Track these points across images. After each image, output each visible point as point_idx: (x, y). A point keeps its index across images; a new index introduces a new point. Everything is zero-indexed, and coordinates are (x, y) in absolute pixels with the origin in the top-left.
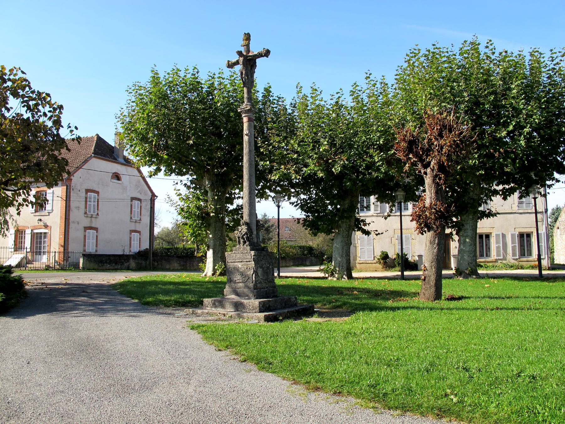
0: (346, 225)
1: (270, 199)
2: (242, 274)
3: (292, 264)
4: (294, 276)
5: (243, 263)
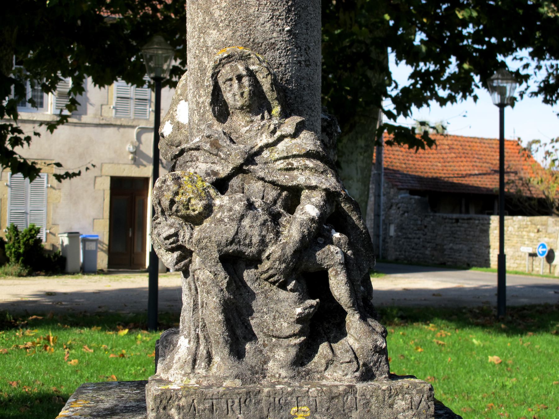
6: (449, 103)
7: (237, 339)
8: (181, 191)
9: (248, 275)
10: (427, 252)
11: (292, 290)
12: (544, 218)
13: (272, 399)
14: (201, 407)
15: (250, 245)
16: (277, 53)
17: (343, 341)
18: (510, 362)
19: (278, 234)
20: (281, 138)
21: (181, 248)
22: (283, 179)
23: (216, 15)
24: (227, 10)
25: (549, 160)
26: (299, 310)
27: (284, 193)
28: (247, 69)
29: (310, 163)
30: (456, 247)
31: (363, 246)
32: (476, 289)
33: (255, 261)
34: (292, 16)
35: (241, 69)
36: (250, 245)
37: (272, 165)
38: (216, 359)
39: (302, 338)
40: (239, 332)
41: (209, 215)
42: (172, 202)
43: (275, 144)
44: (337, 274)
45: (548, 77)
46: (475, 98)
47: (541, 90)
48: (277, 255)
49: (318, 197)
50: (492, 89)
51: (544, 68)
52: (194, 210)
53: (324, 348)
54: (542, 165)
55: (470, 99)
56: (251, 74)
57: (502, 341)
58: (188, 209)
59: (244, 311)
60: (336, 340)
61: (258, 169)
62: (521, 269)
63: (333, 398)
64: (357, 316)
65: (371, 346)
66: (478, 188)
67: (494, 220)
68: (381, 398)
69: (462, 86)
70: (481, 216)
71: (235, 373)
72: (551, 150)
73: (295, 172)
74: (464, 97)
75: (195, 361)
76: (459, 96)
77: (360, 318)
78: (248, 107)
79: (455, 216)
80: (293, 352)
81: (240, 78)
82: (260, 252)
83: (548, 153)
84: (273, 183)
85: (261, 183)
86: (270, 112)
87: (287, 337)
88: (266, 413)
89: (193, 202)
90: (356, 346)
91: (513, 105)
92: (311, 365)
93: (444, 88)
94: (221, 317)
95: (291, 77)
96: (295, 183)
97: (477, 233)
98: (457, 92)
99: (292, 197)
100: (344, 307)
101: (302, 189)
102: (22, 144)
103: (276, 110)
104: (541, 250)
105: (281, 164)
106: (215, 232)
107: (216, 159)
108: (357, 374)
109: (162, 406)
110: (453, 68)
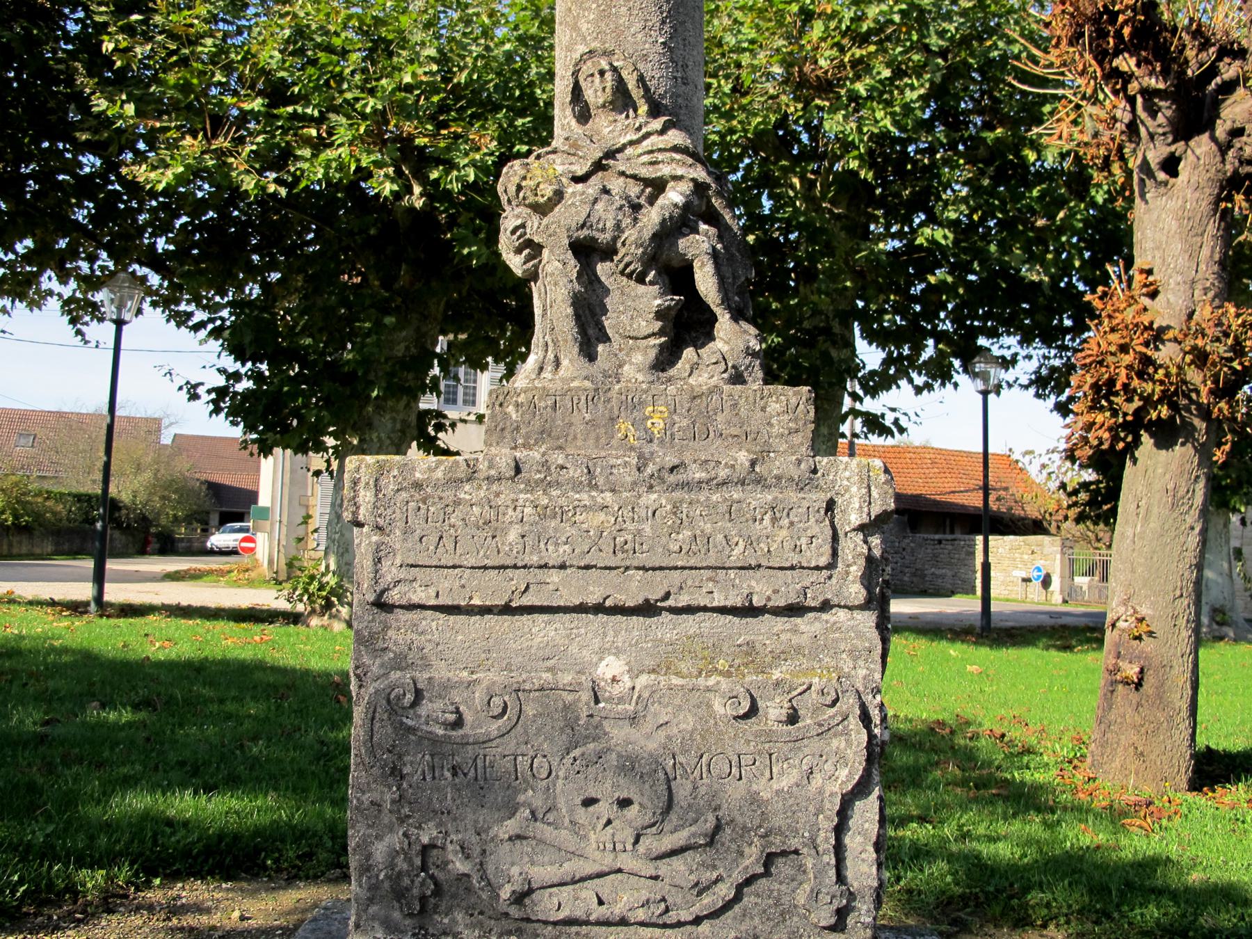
0: (394, 420)
1: (53, 304)
2: (660, 790)
3: (50, 548)
4: (157, 600)
5: (665, 628)
6: (925, 392)
7: (589, 340)
8: (529, 175)
9: (602, 269)
10: (906, 579)
11: (652, 283)
12: (1040, 537)
13: (624, 397)
14: (543, 404)
15: (603, 230)
16: (650, 65)
17: (711, 345)
18: (991, 672)
19: (635, 220)
20: (647, 135)
21: (529, 243)
22: (646, 172)
23: (584, 29)
24: (596, 22)
25: (1045, 472)
26: (658, 302)
27: (648, 190)
28: (611, 64)
29: (678, 156)
30: (938, 572)
31: (739, 251)
32: (959, 614)
33: (608, 253)
34: (667, 28)
35: (604, 64)
36: (603, 230)
37: (636, 161)
38: (565, 363)
39: (663, 339)
40: (591, 332)
41: (559, 202)
42: (519, 188)
43: (638, 142)
44: (703, 265)
45: (1040, 367)
46: (956, 385)
47: (1032, 383)
48: (633, 238)
49: (686, 187)
50: (975, 375)
51: (1035, 358)
52: (543, 196)
53: (689, 353)
54: (1037, 481)
55: (949, 386)
56: (615, 69)
57: (984, 652)
58: (536, 195)
59: (598, 310)
60: (703, 345)
61: (620, 164)
62: (1013, 596)
63: (695, 398)
64: (728, 316)
65: (742, 347)
66: (963, 506)
67: (979, 539)
68: (751, 399)
69: (940, 372)
70: (967, 537)
71: (584, 374)
72: (1047, 462)
73: (661, 166)
74: (943, 384)
75: (541, 369)
76: (937, 385)
77: (731, 318)
78: (611, 103)
79: (937, 537)
80: (652, 354)
81: (602, 73)
82: (615, 239)
83: (1044, 466)
84: (634, 177)
85: (622, 179)
86: (635, 110)
87: (645, 338)
88: (617, 413)
89: (542, 186)
90: (725, 348)
91: (998, 394)
92: (672, 372)
93: (920, 374)
94: (570, 310)
95: (666, 92)
96: (659, 174)
97: (963, 556)
98: (934, 379)
99: (658, 186)
100: (712, 306)
101: (667, 182)
102: (446, 431)
103: (643, 108)
104: (1036, 574)
105: (645, 158)
106: (567, 217)
107: (573, 159)
108: (725, 375)
109: (498, 403)
110: (929, 352)
